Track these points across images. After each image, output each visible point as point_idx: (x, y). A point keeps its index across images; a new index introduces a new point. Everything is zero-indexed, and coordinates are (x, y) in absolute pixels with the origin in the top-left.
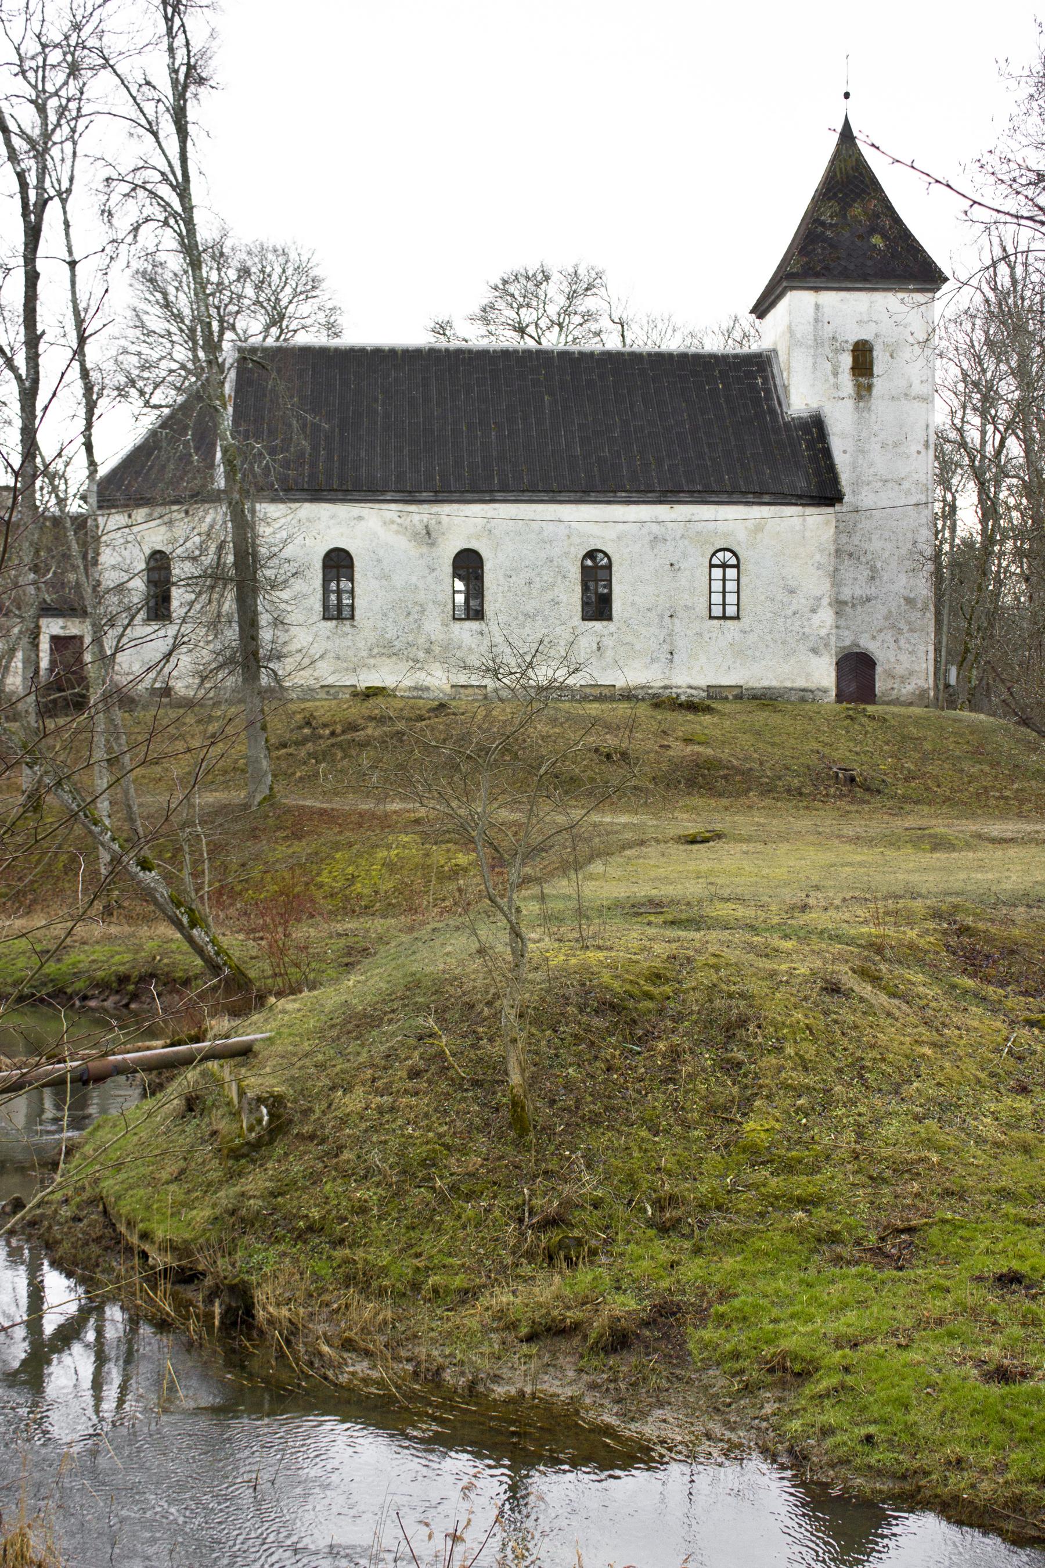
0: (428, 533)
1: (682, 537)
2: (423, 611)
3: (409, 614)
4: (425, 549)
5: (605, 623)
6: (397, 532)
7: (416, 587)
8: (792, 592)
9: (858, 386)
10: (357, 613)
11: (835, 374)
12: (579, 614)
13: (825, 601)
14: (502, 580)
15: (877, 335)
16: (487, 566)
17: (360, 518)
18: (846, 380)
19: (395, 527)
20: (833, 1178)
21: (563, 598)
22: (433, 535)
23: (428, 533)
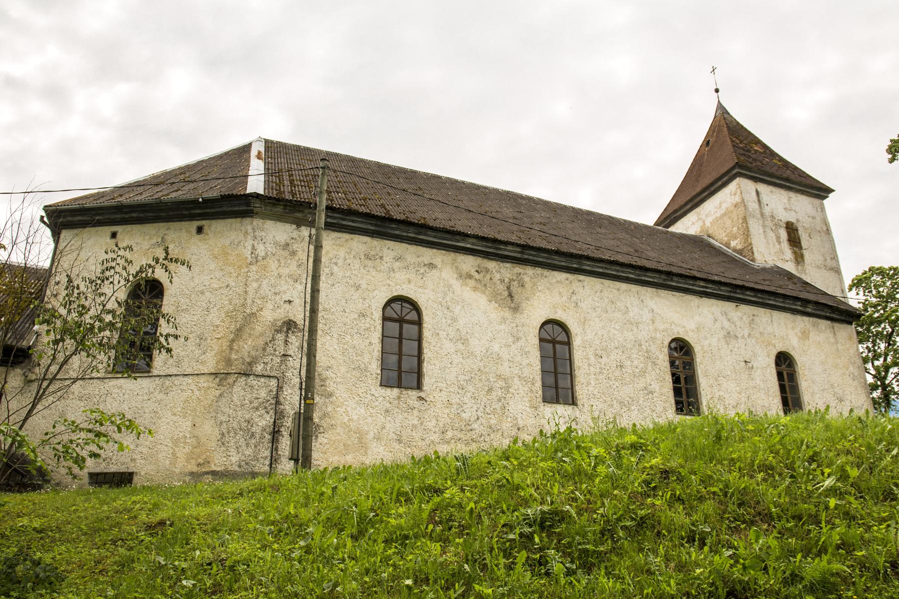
0: (510, 295)
3: (490, 390)
6: (475, 289)
9: (795, 253)
10: (427, 382)
14: (592, 359)
15: (798, 220)
18: (786, 246)
19: (472, 283)
22: (516, 297)
23: (510, 295)
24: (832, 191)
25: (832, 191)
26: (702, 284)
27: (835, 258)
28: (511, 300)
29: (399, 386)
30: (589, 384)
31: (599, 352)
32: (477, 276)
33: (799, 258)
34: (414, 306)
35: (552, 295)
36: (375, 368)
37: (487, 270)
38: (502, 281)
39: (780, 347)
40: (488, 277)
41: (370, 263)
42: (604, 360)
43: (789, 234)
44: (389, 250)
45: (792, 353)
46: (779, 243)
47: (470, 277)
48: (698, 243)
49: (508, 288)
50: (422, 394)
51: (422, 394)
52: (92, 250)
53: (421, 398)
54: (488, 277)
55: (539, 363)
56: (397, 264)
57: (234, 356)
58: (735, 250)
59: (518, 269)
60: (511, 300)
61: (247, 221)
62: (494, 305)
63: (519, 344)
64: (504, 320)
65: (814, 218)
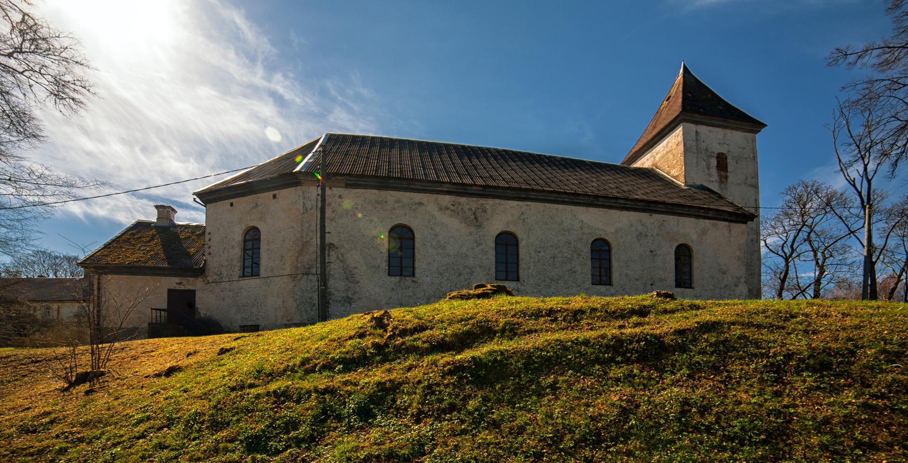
0: (476, 218)
1: (657, 234)
2: (471, 273)
3: (460, 274)
4: (472, 229)
5: (608, 287)
6: (451, 216)
7: (467, 256)
8: (724, 273)
9: (720, 176)
10: (417, 271)
11: (709, 169)
12: (590, 280)
13: (743, 280)
14: (533, 254)
15: (729, 151)
16: (522, 244)
17: (421, 204)
18: (714, 171)
19: (449, 212)
20: (457, 448)
21: (579, 268)
22: (480, 219)
23: (476, 218)
24: (766, 125)
25: (766, 125)
26: (622, 201)
27: (756, 176)
28: (476, 220)
29: (401, 275)
30: (529, 268)
31: (538, 249)
32: (452, 207)
33: (723, 179)
34: (410, 230)
35: (504, 215)
36: (384, 266)
37: (460, 204)
38: (470, 209)
39: (681, 241)
40: (460, 208)
41: (379, 206)
42: (542, 254)
43: (718, 162)
44: (391, 196)
45: (690, 244)
46: (709, 169)
47: (447, 209)
48: (648, 174)
49: (474, 214)
50: (415, 279)
51: (415, 279)
52: (239, 216)
53: (414, 281)
54: (460, 208)
55: (494, 258)
56: (396, 205)
57: (299, 265)
58: (673, 177)
59: (482, 201)
60: (476, 220)
61: (299, 188)
62: (463, 225)
63: (480, 247)
64: (471, 234)
65: (743, 148)
